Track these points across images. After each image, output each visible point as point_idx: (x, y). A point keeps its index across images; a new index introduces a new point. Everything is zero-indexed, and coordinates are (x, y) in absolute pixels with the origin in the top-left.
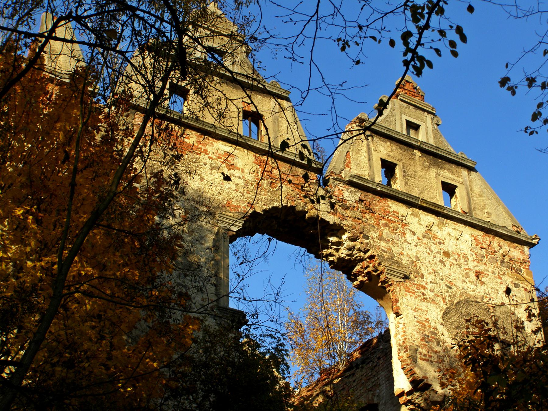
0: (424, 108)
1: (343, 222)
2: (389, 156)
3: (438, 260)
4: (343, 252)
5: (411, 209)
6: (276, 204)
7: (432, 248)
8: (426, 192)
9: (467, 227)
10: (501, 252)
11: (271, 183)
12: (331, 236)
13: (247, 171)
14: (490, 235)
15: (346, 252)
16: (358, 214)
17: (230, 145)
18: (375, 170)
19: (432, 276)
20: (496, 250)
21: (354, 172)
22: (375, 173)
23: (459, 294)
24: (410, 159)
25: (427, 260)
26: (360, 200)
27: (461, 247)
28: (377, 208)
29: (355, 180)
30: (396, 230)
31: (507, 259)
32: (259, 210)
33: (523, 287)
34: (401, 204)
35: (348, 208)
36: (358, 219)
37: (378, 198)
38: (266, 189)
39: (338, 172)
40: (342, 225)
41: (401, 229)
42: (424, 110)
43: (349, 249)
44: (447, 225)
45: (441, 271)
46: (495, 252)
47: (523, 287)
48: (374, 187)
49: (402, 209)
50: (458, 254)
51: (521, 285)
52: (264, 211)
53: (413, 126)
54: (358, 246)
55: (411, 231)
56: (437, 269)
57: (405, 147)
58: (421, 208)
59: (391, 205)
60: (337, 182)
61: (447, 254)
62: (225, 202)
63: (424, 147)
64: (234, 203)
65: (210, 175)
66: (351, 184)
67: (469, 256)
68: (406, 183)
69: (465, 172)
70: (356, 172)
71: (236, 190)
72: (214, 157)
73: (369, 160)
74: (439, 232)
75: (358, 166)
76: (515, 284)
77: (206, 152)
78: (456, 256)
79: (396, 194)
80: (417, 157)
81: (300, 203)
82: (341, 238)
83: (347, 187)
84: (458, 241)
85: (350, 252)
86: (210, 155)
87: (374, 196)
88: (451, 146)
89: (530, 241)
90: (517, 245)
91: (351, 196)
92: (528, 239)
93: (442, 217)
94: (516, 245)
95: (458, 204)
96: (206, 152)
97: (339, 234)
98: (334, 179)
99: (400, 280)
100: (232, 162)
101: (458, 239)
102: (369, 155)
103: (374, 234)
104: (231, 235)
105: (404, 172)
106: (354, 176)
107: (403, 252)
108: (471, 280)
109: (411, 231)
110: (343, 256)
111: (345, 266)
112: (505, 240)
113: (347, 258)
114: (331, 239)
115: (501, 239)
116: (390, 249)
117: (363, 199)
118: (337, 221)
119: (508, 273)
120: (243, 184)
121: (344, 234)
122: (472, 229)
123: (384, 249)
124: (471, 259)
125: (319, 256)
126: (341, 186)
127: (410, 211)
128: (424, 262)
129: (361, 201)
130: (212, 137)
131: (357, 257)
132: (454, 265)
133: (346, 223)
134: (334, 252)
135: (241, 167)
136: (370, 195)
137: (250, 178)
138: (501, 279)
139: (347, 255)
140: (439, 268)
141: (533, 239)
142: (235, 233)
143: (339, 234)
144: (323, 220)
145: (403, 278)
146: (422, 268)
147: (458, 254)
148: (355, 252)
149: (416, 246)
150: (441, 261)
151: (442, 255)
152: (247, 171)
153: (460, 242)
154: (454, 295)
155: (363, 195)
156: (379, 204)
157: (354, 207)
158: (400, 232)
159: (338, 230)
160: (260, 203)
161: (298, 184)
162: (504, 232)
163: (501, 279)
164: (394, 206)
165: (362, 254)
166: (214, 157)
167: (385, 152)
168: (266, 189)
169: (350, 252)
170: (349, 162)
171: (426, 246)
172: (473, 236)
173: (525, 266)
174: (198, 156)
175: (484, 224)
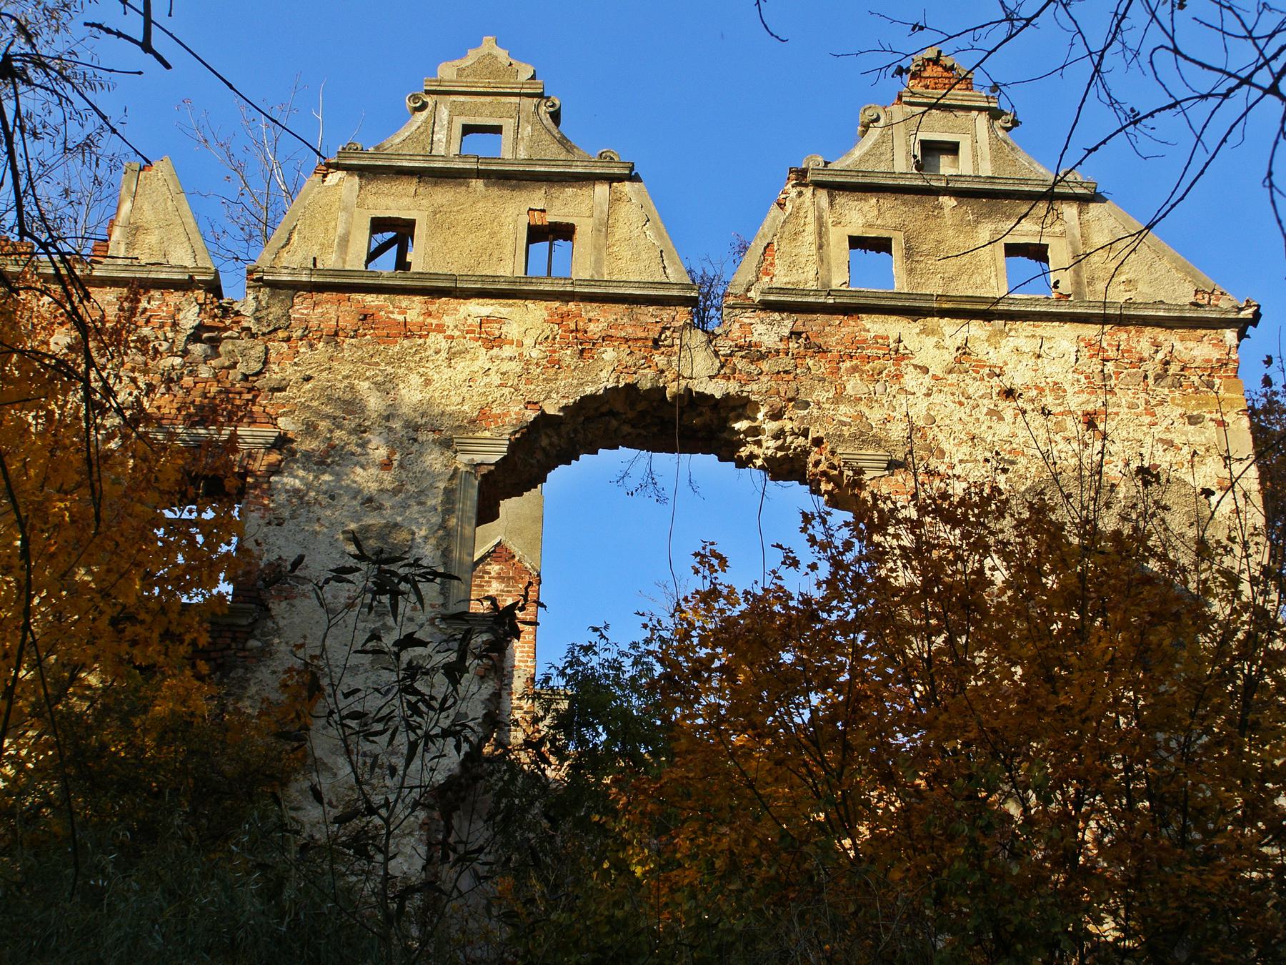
0: (966, 103)
1: (747, 388)
2: (871, 226)
3: (985, 410)
4: (769, 446)
5: (921, 321)
6: (589, 390)
7: (971, 391)
8: (965, 277)
9: (1067, 326)
10: (1160, 356)
11: (582, 351)
12: (737, 419)
13: (528, 342)
14: (1131, 328)
15: (772, 444)
16: (785, 362)
17: (493, 301)
18: (833, 264)
19: (965, 449)
20: (1146, 355)
21: (781, 280)
22: (834, 269)
23: (1033, 470)
24: (927, 218)
25: (955, 418)
26: (792, 333)
27: (1048, 371)
28: (832, 341)
29: (772, 298)
30: (880, 373)
31: (1174, 369)
32: (551, 410)
33: (1212, 420)
34: (894, 318)
35: (762, 357)
36: (786, 372)
37: (836, 320)
38: (568, 366)
39: (740, 291)
40: (745, 394)
41: (893, 369)
42: (969, 109)
43: (776, 437)
44: (1012, 333)
45: (992, 431)
46: (1141, 360)
47: (1212, 420)
48: (821, 300)
49: (893, 327)
50: (1037, 387)
51: (1208, 416)
52: (563, 409)
53: (932, 150)
54: (788, 426)
55: (916, 367)
56: (981, 430)
57: (916, 197)
58: (943, 313)
59: (868, 327)
60: (737, 311)
61: (1009, 393)
62: (475, 414)
63: (958, 185)
64: (496, 410)
65: (446, 370)
66: (768, 306)
67: (1066, 387)
68: (911, 271)
69: (1070, 211)
70: (787, 280)
71: (501, 385)
72: (457, 333)
73: (820, 247)
74: (992, 350)
75: (793, 265)
76: (1190, 418)
77: (440, 328)
78: (1034, 393)
79: (862, 301)
80: (947, 210)
81: (645, 375)
82: (755, 419)
83: (763, 315)
84: (1039, 361)
85: (780, 442)
86: (448, 333)
87: (827, 317)
88: (1040, 162)
89: (1232, 316)
90: (1204, 332)
91: (768, 332)
92: (1226, 312)
93: (1000, 318)
94: (1201, 332)
95: (581, 262)
96: (440, 328)
97: (749, 413)
98: (729, 307)
99: (880, 474)
100: (497, 333)
101: (1039, 356)
102: (820, 238)
103: (822, 394)
104: (485, 472)
105: (908, 249)
106: (771, 290)
107: (893, 414)
108: (1068, 434)
109: (916, 367)
110: (769, 452)
111: (786, 467)
112: (1172, 328)
113: (780, 454)
114: (737, 426)
115: (1159, 330)
116: (862, 415)
117: (801, 329)
118: (733, 387)
119: (1173, 399)
120: (518, 370)
121: (758, 410)
122: (1080, 325)
123: (844, 419)
124: (1070, 390)
125: (742, 463)
126: (747, 317)
127: (916, 326)
128: (948, 422)
129: (795, 334)
130: (456, 297)
131: (795, 448)
132: (1024, 412)
133: (754, 390)
134: (756, 450)
135: (687, 334)
136: (821, 318)
137: (535, 354)
138: (1153, 415)
139: (778, 449)
140: (984, 427)
141: (1242, 309)
142: (492, 468)
143: (749, 413)
144: (701, 395)
145: (886, 469)
146: (940, 437)
147: (1037, 387)
148: (789, 439)
149: (929, 395)
150: (991, 413)
151: (995, 398)
152: (528, 342)
153: (1046, 361)
154: (1020, 476)
155: (800, 323)
156: (837, 331)
157: (778, 352)
158: (888, 376)
159: (742, 406)
160: (554, 395)
161: (646, 339)
162: (1161, 313)
163: (1153, 415)
164: (874, 326)
165: (801, 440)
166: (457, 333)
167: (861, 221)
168: (568, 366)
169: (780, 442)
170: (771, 264)
171: (954, 389)
172: (1083, 340)
173: (1226, 371)
174: (421, 341)
175: (1027, 305)
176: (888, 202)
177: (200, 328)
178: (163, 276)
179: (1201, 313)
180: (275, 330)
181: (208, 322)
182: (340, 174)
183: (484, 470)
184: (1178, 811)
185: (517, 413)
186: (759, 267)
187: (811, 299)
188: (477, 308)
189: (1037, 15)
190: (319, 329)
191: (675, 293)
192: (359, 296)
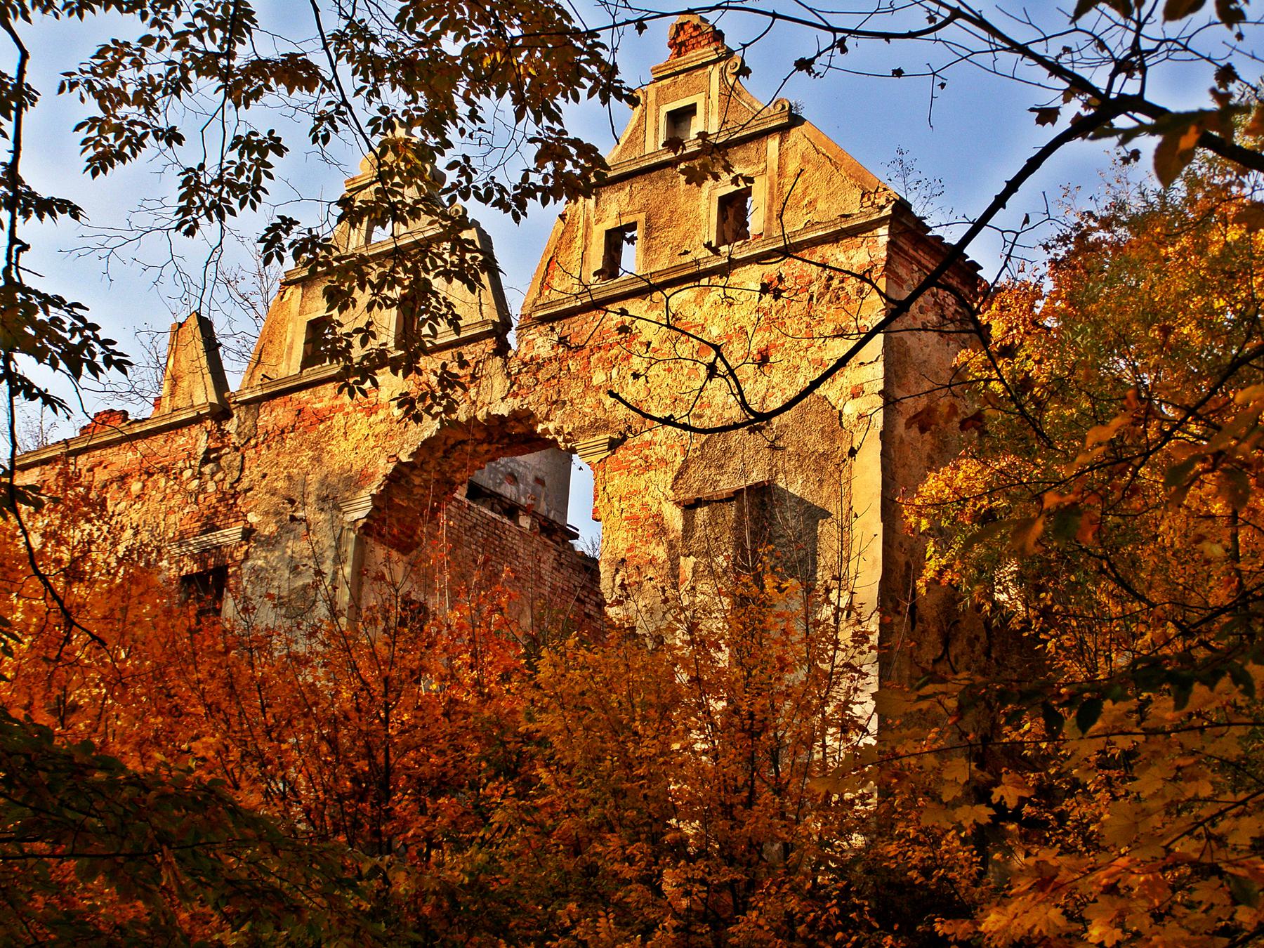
87: (584, 316)
141: (883, 207)
157: (550, 359)
162: (820, 233)
176: (639, 184)
177: (208, 451)
178: (183, 417)
179: (851, 223)
180: (249, 440)
181: (213, 445)
182: (292, 287)
183: (360, 524)
184: (42, 552)
185: (384, 467)
186: (542, 284)
187: (567, 306)
188: (616, 307)
189: (14, 445)
190: (274, 431)
191: (478, 331)
192: (295, 395)
